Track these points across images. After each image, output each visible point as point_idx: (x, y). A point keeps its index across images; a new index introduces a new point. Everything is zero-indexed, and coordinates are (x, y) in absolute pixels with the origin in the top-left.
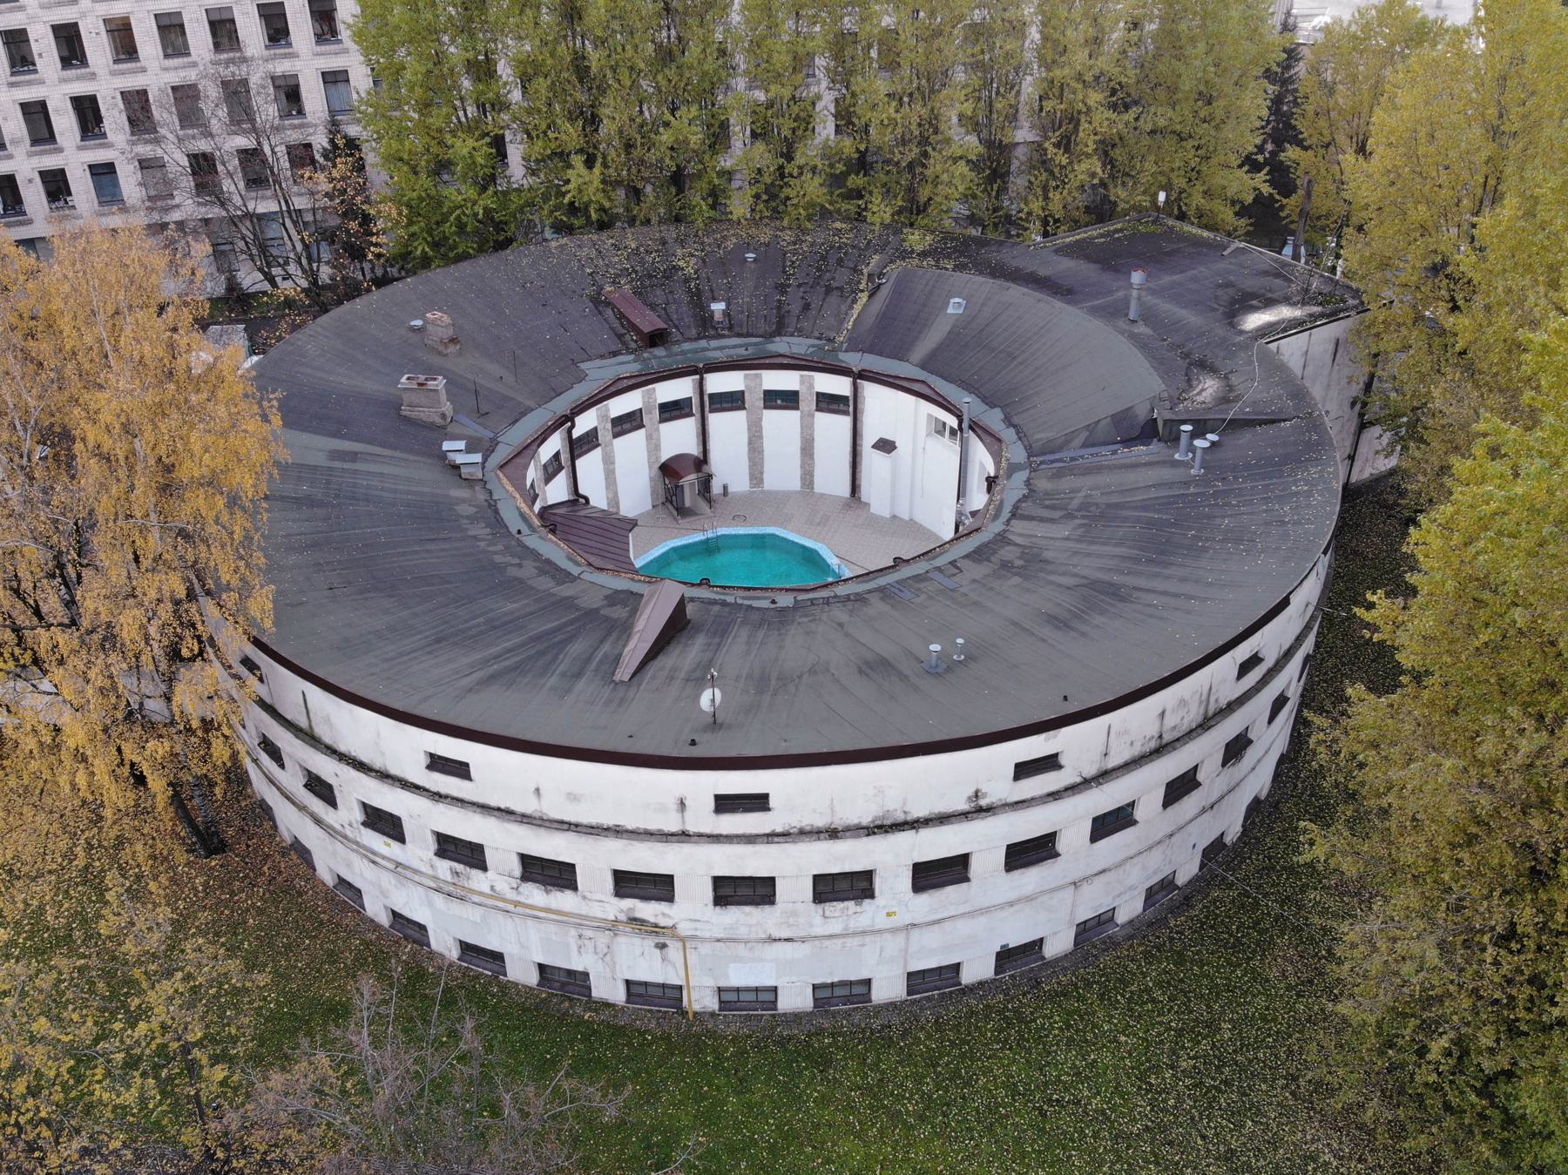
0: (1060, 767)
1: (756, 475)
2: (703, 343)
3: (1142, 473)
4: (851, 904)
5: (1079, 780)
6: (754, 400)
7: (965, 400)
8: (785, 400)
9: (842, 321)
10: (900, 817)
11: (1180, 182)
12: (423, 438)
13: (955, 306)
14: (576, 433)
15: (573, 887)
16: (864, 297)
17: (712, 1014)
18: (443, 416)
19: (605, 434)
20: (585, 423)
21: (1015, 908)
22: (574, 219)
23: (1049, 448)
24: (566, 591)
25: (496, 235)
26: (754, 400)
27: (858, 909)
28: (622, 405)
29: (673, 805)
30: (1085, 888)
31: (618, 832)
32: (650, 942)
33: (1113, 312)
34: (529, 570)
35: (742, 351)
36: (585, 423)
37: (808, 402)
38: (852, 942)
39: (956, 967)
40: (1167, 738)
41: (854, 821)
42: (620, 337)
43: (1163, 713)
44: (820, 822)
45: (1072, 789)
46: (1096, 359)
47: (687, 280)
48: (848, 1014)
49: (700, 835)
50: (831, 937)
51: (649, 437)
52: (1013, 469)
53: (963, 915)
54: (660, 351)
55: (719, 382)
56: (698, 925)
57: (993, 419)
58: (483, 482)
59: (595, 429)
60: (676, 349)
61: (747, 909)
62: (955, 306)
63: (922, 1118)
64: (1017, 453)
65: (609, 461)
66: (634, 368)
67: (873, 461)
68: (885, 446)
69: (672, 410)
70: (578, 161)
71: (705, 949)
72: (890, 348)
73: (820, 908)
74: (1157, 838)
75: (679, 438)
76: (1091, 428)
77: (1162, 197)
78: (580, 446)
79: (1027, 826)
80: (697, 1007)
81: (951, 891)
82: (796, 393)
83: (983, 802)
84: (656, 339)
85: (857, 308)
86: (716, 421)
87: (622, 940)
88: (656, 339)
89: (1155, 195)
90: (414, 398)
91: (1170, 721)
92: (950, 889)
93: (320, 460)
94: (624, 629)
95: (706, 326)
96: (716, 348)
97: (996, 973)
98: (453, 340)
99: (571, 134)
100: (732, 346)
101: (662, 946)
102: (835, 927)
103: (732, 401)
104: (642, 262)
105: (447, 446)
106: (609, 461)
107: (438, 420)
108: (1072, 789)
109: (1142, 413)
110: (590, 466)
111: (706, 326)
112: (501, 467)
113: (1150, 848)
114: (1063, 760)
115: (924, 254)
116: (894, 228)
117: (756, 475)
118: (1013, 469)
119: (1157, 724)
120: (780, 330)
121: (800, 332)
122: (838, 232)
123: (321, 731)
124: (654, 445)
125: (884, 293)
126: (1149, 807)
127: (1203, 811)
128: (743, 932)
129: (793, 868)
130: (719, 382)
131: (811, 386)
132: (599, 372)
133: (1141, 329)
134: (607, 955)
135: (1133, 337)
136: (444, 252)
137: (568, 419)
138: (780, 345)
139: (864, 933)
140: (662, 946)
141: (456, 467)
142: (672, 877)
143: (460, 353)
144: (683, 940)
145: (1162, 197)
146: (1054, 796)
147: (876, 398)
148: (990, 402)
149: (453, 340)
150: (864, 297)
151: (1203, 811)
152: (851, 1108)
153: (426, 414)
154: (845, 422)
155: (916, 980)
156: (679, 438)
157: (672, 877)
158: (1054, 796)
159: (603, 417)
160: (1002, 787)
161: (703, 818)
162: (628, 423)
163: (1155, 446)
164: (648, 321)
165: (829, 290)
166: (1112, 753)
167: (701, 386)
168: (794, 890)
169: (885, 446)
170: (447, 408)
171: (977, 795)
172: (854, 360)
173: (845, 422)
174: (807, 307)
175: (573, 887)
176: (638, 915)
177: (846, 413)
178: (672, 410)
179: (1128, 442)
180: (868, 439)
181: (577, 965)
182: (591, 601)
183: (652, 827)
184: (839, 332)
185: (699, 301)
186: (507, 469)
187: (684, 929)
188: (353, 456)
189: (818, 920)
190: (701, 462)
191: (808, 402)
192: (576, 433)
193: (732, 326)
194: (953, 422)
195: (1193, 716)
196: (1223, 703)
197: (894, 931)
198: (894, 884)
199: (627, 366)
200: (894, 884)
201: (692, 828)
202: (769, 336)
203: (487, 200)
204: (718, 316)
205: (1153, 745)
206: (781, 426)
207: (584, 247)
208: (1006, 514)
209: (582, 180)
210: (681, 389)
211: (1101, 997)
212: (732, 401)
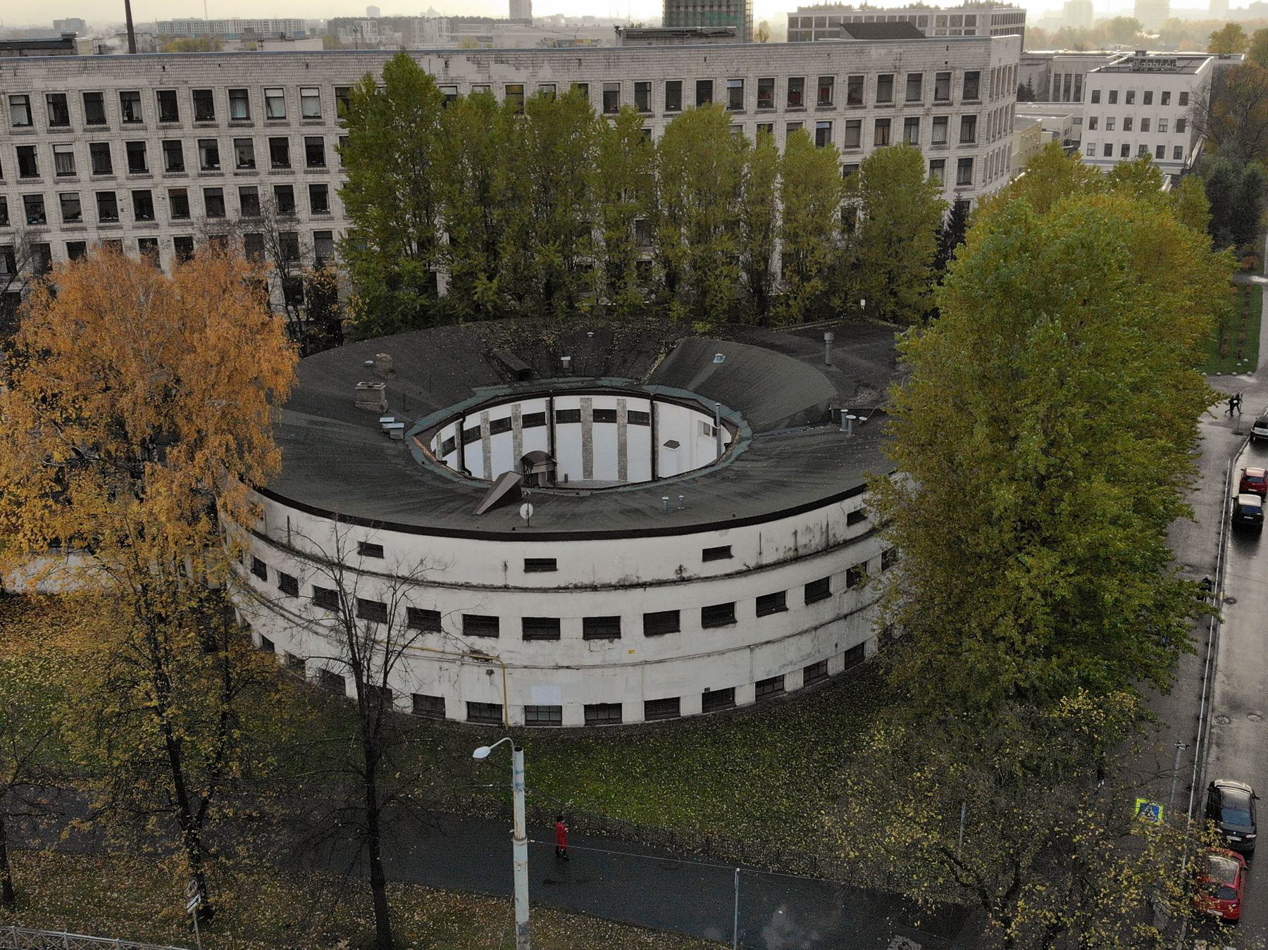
0: (731, 557)
1: (588, 471)
2: (555, 380)
3: (821, 435)
4: (606, 641)
5: (744, 568)
6: (587, 415)
7: (716, 406)
8: (606, 416)
9: (646, 370)
10: (635, 581)
11: (877, 295)
12: (371, 418)
13: (718, 359)
14: (466, 427)
15: (438, 629)
16: (662, 357)
17: (521, 728)
18: (382, 407)
19: (485, 431)
20: (472, 421)
21: (711, 659)
22: (478, 312)
23: (765, 429)
24: (449, 486)
25: (423, 319)
26: (587, 415)
27: (611, 646)
28: (498, 413)
29: (501, 567)
30: (758, 652)
31: (467, 586)
32: (483, 669)
33: (817, 361)
34: (427, 478)
35: (580, 384)
36: (472, 421)
37: (622, 418)
38: (610, 671)
39: (676, 701)
40: (801, 552)
41: (606, 581)
42: (500, 375)
43: (795, 533)
44: (587, 581)
45: (740, 574)
46: (798, 381)
47: (547, 347)
48: (606, 729)
49: (516, 588)
50: (594, 667)
51: (515, 437)
52: (742, 439)
53: (677, 659)
54: (525, 384)
55: (564, 403)
56: (513, 655)
57: (736, 417)
58: (403, 441)
59: (479, 427)
60: (536, 382)
61: (543, 642)
62: (718, 359)
63: (645, 775)
64: (746, 431)
65: (487, 450)
66: (509, 391)
67: (663, 451)
68: (673, 444)
69: (532, 420)
70: (482, 276)
71: (517, 674)
72: (679, 384)
73: (587, 643)
74: (805, 627)
75: (535, 439)
76: (792, 417)
77: (863, 303)
78: (468, 436)
79: (716, 595)
80: (511, 723)
81: (668, 637)
82: (614, 412)
83: (685, 575)
84: (523, 376)
85: (657, 363)
86: (560, 428)
87: (466, 668)
88: (523, 376)
89: (859, 303)
90: (365, 395)
91: (802, 540)
92: (668, 636)
93: (304, 424)
94: (480, 501)
95: (558, 370)
96: (561, 383)
97: (704, 709)
98: (392, 371)
99: (480, 259)
100: (574, 381)
101: (490, 673)
102: (596, 659)
103: (571, 416)
104: (520, 336)
105: (382, 420)
106: (487, 450)
107: (378, 410)
108: (740, 574)
109: (822, 408)
110: (473, 451)
111: (558, 370)
112: (416, 435)
113: (801, 633)
114: (733, 552)
115: (704, 334)
116: (686, 320)
117: (588, 471)
118: (742, 439)
119: (793, 540)
120: (605, 374)
121: (619, 376)
122: (650, 322)
123: (298, 543)
124: (518, 445)
125: (673, 355)
126: (795, 599)
127: (838, 619)
128: (540, 661)
129: (572, 612)
130: (564, 403)
131: (624, 407)
132: (483, 393)
133: (833, 369)
134: (455, 683)
135: (827, 373)
136: (390, 328)
137: (462, 415)
138: (605, 381)
139: (615, 665)
140: (490, 673)
141: (387, 433)
142: (497, 619)
143: (396, 379)
144: (503, 667)
145: (863, 303)
146: (729, 576)
147: (664, 409)
148: (734, 408)
149: (392, 371)
150: (662, 357)
151: (838, 619)
152: (601, 770)
153: (372, 406)
154: (647, 430)
155: (652, 707)
156: (535, 439)
157: (497, 619)
158: (729, 576)
159: (486, 420)
160: (696, 567)
161: (519, 577)
162: (500, 426)
163: (830, 427)
164: (519, 365)
165: (640, 353)
166: (764, 553)
167: (551, 404)
168: (572, 629)
169: (673, 444)
170: (385, 402)
171: (681, 569)
172: (652, 389)
173: (647, 430)
174: (625, 361)
175: (438, 629)
176: (476, 648)
177: (647, 424)
178: (532, 420)
179: (814, 424)
180: (662, 439)
181: (437, 693)
182: (461, 491)
183: (487, 583)
184: (644, 374)
185: (554, 358)
186: (420, 436)
187: (505, 659)
188: (324, 424)
189: (586, 653)
190: (550, 458)
191: (622, 418)
192: (466, 427)
193: (574, 370)
194: (710, 421)
195: (817, 541)
196: (841, 539)
197: (634, 665)
198: (632, 627)
199: (504, 390)
200: (632, 627)
201: (511, 584)
202: (598, 377)
203: (423, 300)
204: (565, 365)
205: (791, 554)
206: (605, 433)
207: (481, 329)
208: (732, 459)
209: (483, 288)
210: (536, 406)
211: (769, 726)
212: (571, 416)
